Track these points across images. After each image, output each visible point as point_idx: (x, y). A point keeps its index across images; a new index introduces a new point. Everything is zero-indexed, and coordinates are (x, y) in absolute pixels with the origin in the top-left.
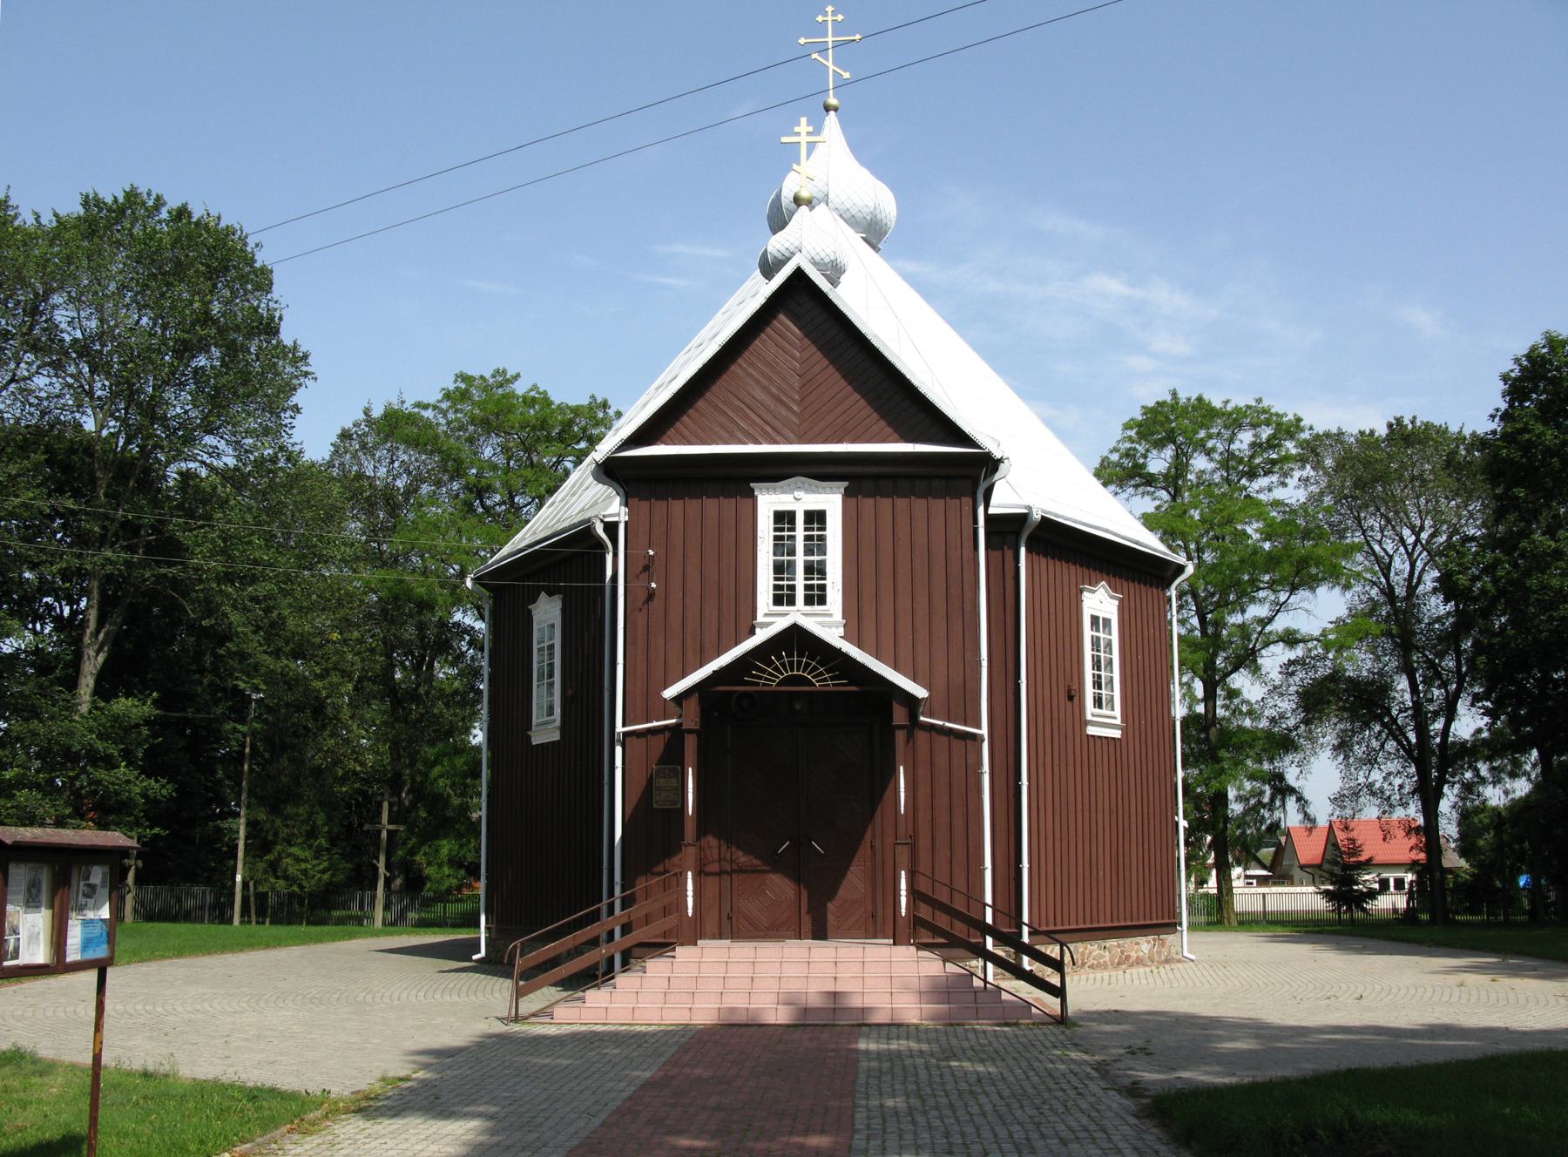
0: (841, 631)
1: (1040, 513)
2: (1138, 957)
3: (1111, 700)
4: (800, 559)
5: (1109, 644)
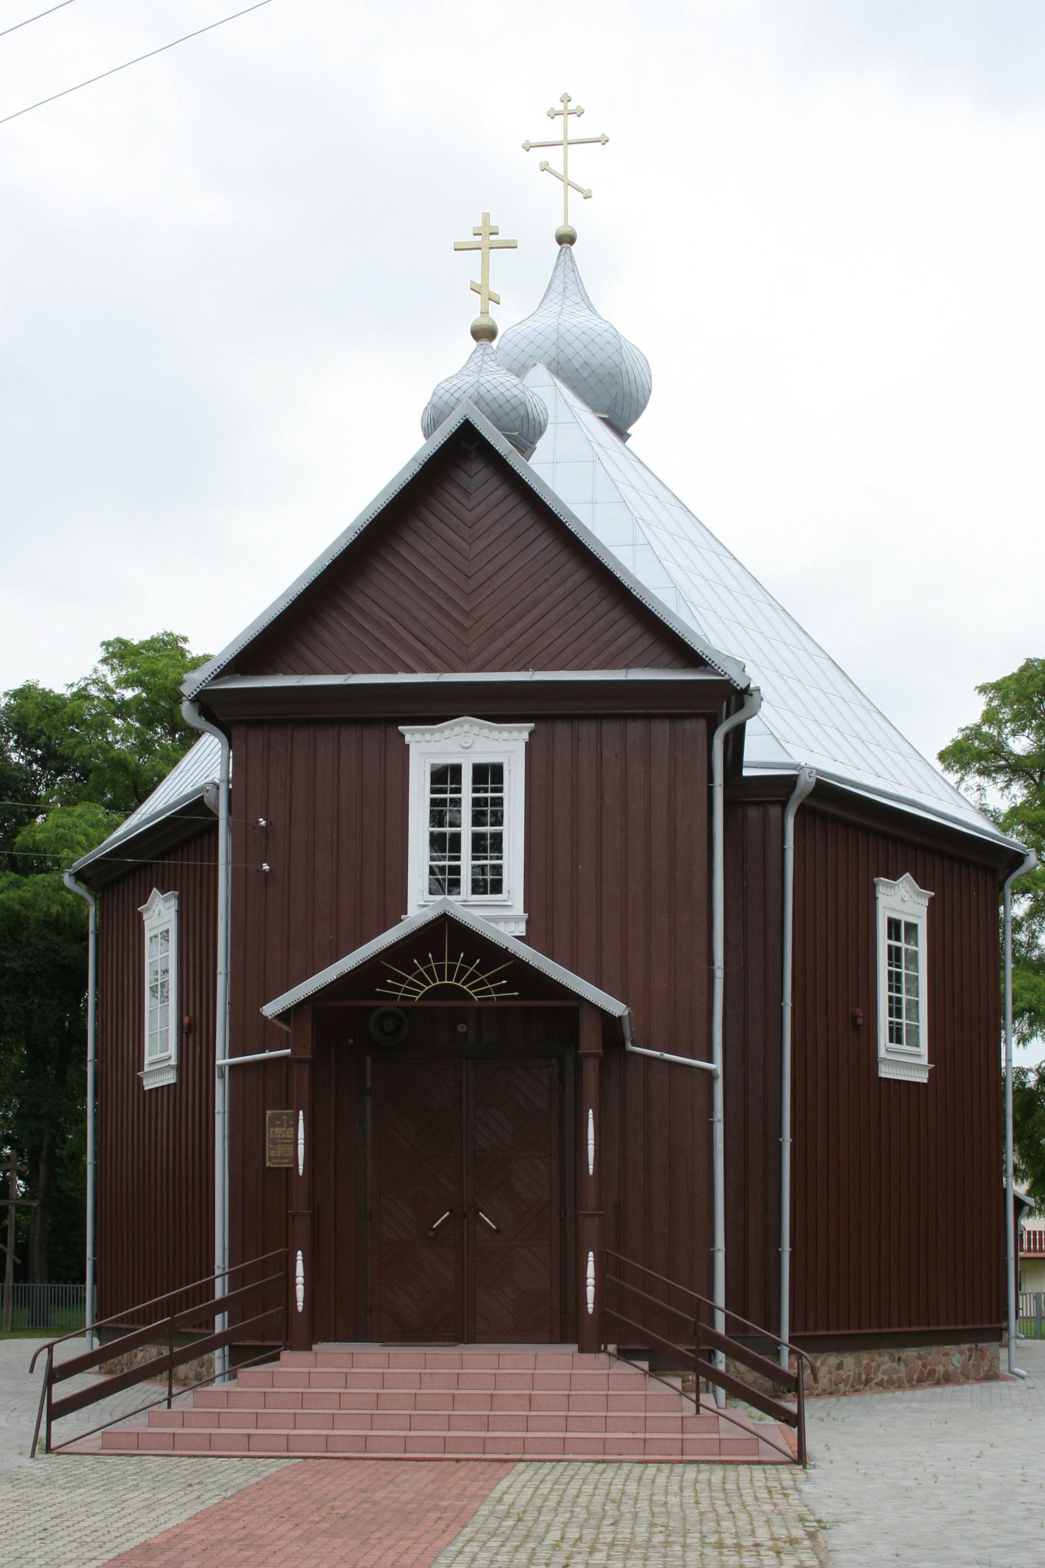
0: (521, 929)
1: (815, 776)
2: (946, 1373)
3: (914, 1031)
4: (466, 831)
5: (913, 957)
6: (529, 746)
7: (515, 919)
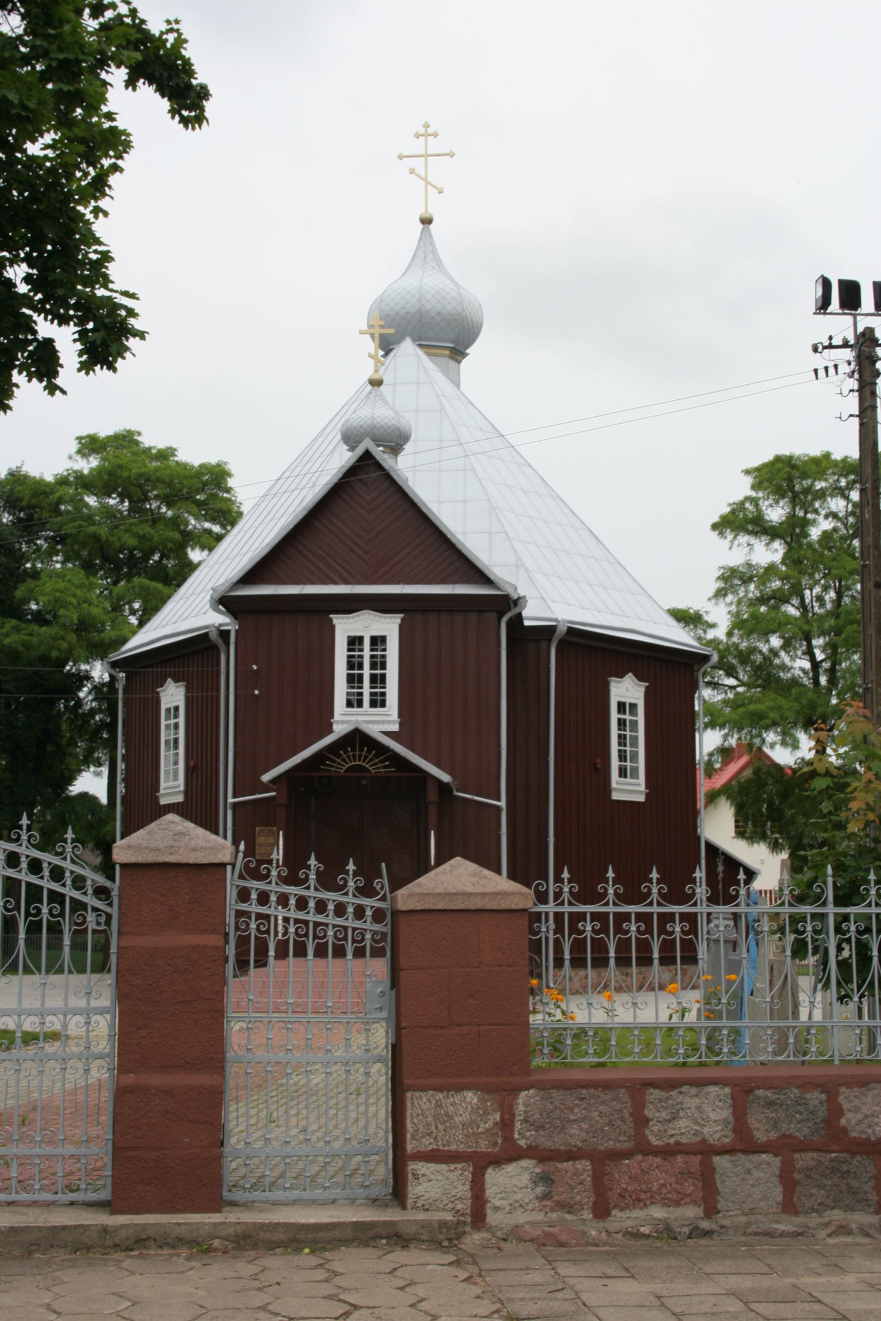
5: (634, 724)
6: (401, 627)
7: (393, 722)
